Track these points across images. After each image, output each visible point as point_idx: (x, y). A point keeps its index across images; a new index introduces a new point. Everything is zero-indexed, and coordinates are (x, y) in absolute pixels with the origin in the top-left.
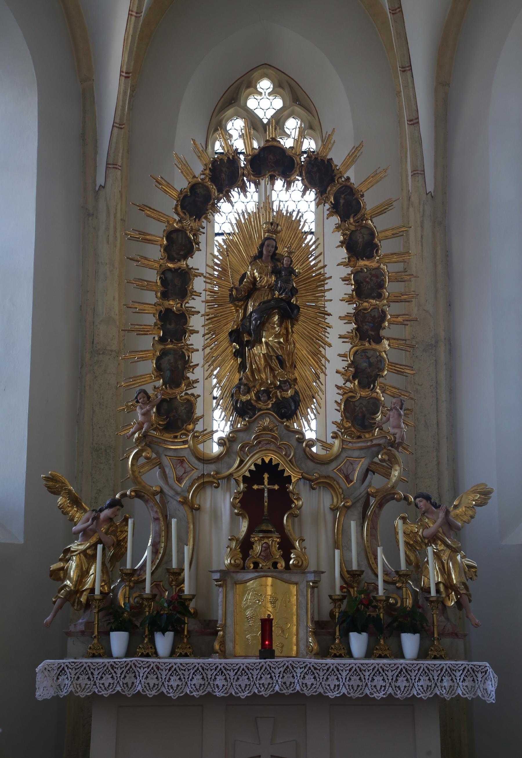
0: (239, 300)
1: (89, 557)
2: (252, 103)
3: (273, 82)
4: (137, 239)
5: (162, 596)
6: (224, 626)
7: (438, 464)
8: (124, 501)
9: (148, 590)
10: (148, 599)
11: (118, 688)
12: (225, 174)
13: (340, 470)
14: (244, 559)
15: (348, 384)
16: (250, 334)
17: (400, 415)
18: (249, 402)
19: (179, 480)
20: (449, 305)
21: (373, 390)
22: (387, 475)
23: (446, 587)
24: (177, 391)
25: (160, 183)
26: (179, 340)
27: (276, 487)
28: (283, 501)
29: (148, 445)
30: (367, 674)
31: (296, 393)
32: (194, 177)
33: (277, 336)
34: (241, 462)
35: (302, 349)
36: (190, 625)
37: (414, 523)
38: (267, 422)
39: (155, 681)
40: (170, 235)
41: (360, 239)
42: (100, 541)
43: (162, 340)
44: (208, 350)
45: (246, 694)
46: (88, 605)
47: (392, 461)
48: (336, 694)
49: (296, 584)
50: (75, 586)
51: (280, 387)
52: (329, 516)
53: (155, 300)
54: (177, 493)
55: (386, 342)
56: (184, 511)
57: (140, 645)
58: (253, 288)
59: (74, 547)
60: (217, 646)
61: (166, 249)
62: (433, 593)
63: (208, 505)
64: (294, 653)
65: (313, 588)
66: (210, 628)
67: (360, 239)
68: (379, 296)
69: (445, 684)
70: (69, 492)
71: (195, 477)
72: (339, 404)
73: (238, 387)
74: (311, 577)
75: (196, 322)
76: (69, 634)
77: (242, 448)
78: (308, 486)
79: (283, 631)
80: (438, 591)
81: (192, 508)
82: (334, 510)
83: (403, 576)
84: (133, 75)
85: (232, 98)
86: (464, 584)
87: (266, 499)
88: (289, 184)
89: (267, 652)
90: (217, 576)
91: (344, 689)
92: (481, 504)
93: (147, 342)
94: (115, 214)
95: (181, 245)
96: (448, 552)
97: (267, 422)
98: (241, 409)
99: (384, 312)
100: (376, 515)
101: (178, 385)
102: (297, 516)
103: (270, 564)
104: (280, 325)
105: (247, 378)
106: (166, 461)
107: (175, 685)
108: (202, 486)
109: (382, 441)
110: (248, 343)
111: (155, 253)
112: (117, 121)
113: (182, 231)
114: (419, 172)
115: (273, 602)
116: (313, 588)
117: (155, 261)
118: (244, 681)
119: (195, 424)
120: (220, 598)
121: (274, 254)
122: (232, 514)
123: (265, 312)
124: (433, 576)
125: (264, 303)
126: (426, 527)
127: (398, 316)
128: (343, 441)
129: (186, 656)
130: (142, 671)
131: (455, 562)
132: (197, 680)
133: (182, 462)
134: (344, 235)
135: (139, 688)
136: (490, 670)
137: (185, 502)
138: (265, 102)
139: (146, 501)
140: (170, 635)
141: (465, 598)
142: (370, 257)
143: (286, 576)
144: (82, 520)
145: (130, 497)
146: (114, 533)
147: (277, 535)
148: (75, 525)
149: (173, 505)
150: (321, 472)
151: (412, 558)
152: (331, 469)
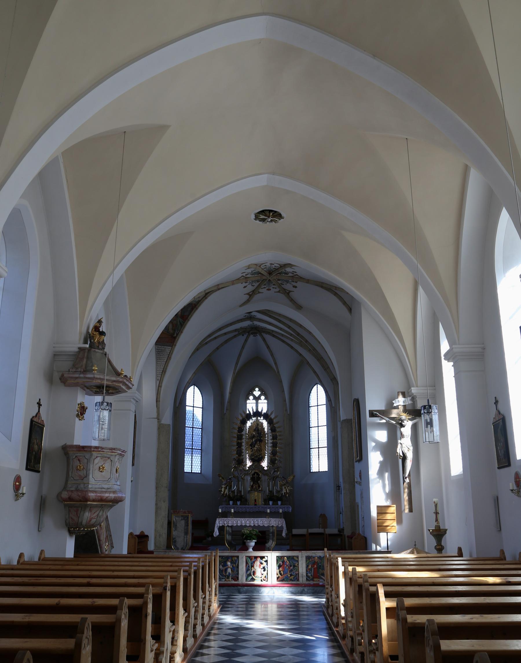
1: (226, 488)
2: (254, 393)
28: (259, 478)
58: (254, 437)
66: (246, 500)
75: (243, 444)
83: (280, 491)
84: (231, 393)
85: (250, 392)
89: (256, 505)
93: (235, 448)
95: (241, 429)
98: (252, 459)
111: (236, 431)
114: (286, 410)
123: (256, 441)
124: (284, 491)
137: (242, 478)
138: (257, 393)
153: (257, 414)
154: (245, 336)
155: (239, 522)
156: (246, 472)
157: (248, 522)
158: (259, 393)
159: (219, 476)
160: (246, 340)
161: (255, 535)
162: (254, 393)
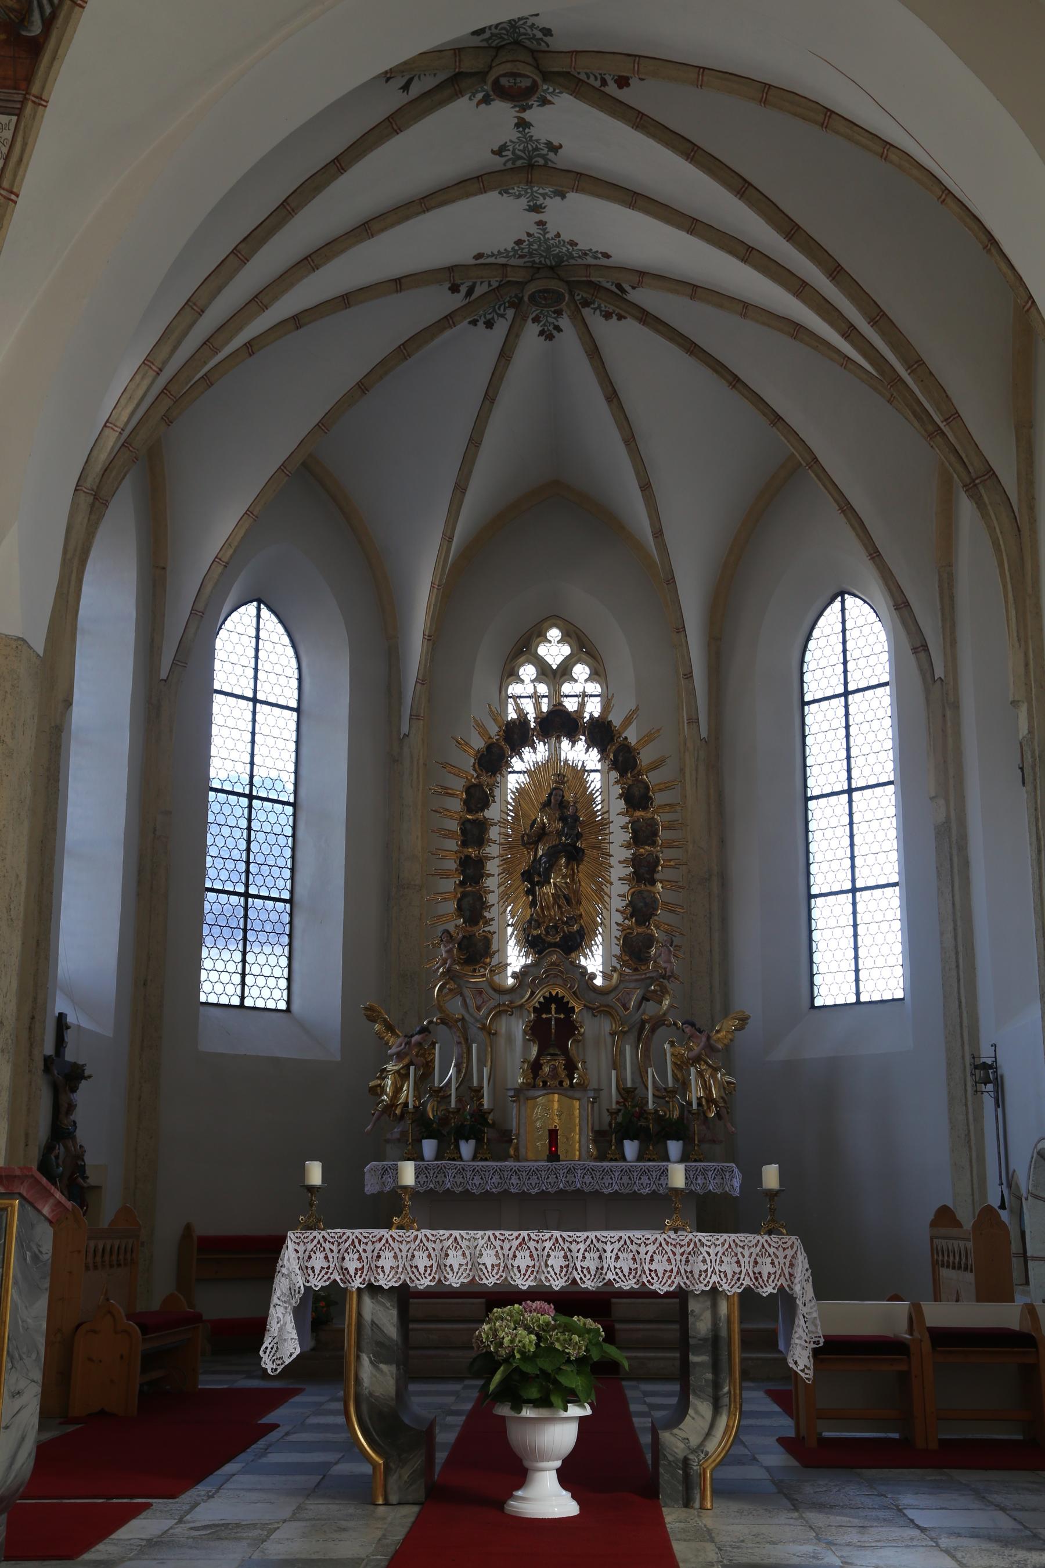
0: (529, 843)
1: (402, 1076)
2: (542, 650)
3: (561, 631)
4: (439, 794)
5: (465, 1110)
6: (518, 1136)
7: (711, 988)
8: (431, 1027)
9: (453, 1104)
10: (453, 1113)
11: (432, 1186)
12: (518, 735)
13: (618, 1000)
14: (534, 1078)
15: (626, 922)
16: (539, 875)
17: (670, 951)
18: (539, 936)
19: (479, 1008)
20: (722, 841)
21: (648, 927)
22: (660, 1003)
23: (708, 1101)
24: (475, 929)
25: (463, 744)
26: (477, 883)
27: (562, 1016)
28: (568, 1028)
29: (451, 978)
30: (635, 1174)
31: (581, 927)
32: (490, 738)
33: (564, 877)
34: (533, 993)
35: (587, 887)
36: (489, 1134)
37: (681, 1045)
38: (554, 958)
39: (461, 1180)
40: (469, 789)
41: (636, 792)
42: (411, 1063)
43: (462, 884)
44: (502, 888)
45: (536, 1190)
46: (402, 1117)
47: (664, 991)
48: (610, 1190)
49: (579, 1099)
50: (391, 1100)
51: (566, 923)
52: (609, 1039)
53: (456, 848)
54: (477, 1020)
55: (659, 885)
56: (482, 1036)
57: (447, 1151)
58: (542, 834)
59: (389, 1067)
60: (512, 1152)
61: (466, 802)
62: (695, 1106)
63: (503, 1030)
64: (577, 1158)
65: (593, 1103)
66: (506, 1137)
67: (636, 792)
68: (654, 843)
69: (699, 1181)
70: (385, 1020)
71: (492, 1006)
72: (619, 940)
73: (529, 922)
74: (591, 1094)
75: (492, 867)
76: (388, 1141)
77: (533, 981)
78: (590, 1014)
79: (567, 1139)
80: (699, 1104)
81: (490, 1033)
82: (613, 1034)
83: (672, 1093)
84: (433, 639)
85: (524, 648)
86: (722, 1098)
87: (553, 1027)
88: (574, 743)
89: (553, 1156)
90: (511, 1093)
91: (782, 1279)
92: (740, 1028)
93: (449, 885)
94: (418, 760)
95: (478, 798)
96: (710, 1071)
97: (554, 958)
98: (532, 943)
99: (657, 857)
100: (649, 1039)
101: (477, 923)
102: (579, 1041)
103: (557, 1082)
104: (566, 867)
105: (538, 914)
106: (467, 993)
107: (477, 1183)
108: (498, 1014)
109: (654, 975)
110: (538, 883)
111: (456, 805)
112: (420, 677)
113: (479, 786)
114: (694, 721)
115: (559, 1116)
116: (593, 1103)
117: (455, 812)
118: (534, 1180)
119: (491, 958)
120: (515, 1112)
121: (561, 802)
122: (525, 1041)
123: (553, 855)
124: (696, 1092)
125: (552, 847)
126: (690, 1049)
127: (670, 860)
128: (621, 974)
129: (486, 1160)
130: (450, 1172)
131: (715, 1079)
132: (496, 1179)
133: (481, 993)
134: (622, 788)
135: (449, 1186)
136: (736, 1170)
137: (484, 1028)
138: (554, 650)
139: (450, 1027)
140: (472, 1142)
141: (724, 1111)
142: (645, 808)
143: (570, 1093)
144: (395, 1044)
145: (436, 1023)
146: (423, 1055)
147: (563, 1057)
148: (390, 1048)
149: (473, 1030)
150: (602, 1002)
151: (679, 1076)
152: (611, 999)
153: (559, 723)
154: (502, 327)
155: (455, 1259)
156: (506, 1001)
157: (523, 1261)
158: (566, 650)
159: (372, 1014)
160: (505, 356)
161: (581, 1361)
162: (542, 650)
